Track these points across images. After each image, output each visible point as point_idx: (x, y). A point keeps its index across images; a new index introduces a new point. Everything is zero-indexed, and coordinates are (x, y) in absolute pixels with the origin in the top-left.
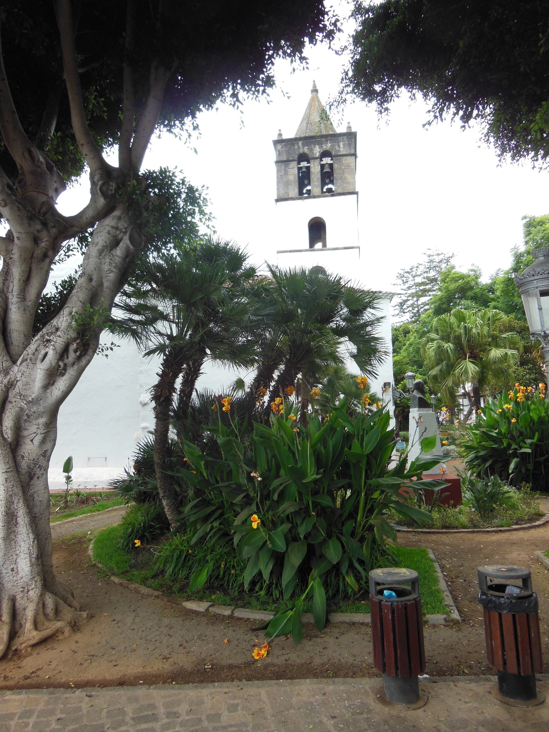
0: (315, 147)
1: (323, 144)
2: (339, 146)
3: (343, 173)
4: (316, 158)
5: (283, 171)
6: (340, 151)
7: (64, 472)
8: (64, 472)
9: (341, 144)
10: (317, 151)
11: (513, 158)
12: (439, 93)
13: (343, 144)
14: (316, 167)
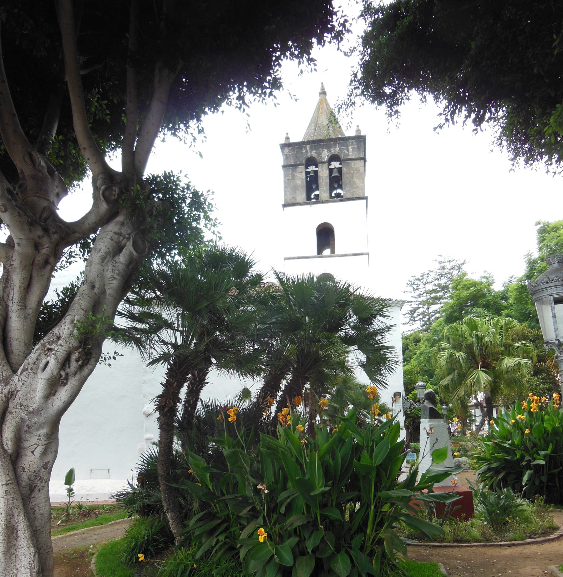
0: (323, 151)
1: (331, 148)
2: (348, 150)
3: (352, 177)
4: (324, 162)
5: (290, 176)
6: (348, 155)
7: (65, 484)
8: (65, 484)
9: (350, 148)
10: (325, 155)
11: (527, 162)
12: (451, 95)
13: (352, 148)
14: (325, 171)
